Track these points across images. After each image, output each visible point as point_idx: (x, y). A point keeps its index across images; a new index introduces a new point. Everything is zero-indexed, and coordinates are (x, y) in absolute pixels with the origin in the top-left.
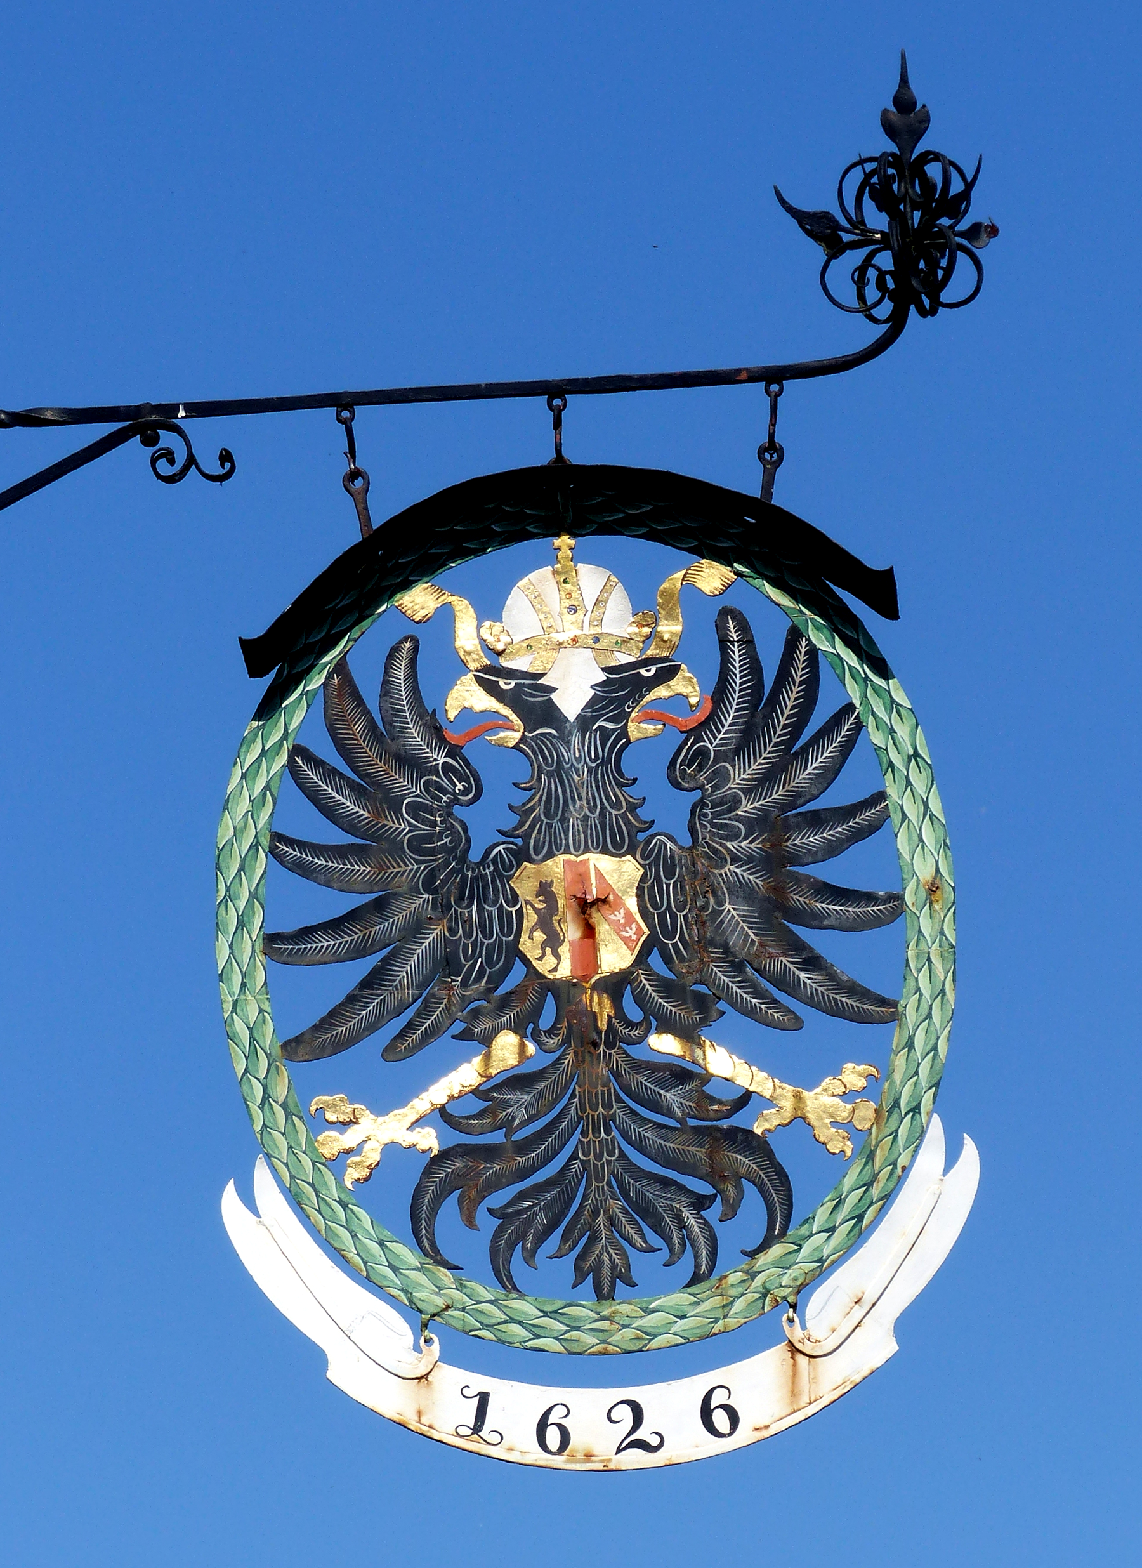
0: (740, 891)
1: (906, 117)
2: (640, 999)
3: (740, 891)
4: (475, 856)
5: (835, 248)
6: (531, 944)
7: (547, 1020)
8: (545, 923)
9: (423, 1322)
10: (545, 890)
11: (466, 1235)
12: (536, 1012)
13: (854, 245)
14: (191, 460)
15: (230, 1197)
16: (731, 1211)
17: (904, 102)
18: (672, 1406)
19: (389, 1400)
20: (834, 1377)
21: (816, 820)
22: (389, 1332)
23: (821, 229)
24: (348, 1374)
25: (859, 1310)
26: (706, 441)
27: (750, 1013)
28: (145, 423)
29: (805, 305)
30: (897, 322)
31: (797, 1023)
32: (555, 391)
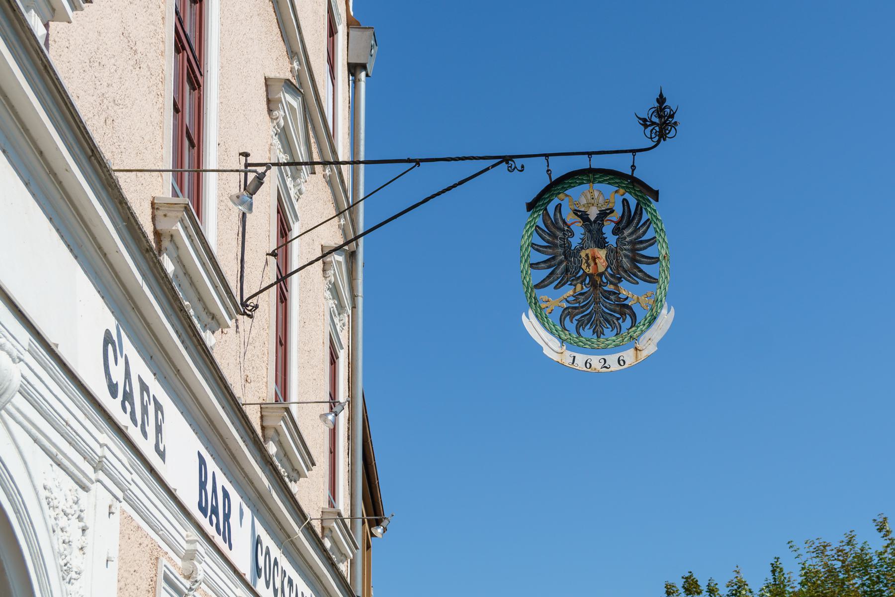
0: (626, 256)
1: (661, 100)
2: (606, 278)
3: (626, 256)
4: (573, 248)
5: (646, 126)
6: (584, 266)
7: (587, 281)
8: (587, 262)
9: (563, 341)
10: (587, 255)
11: (571, 325)
12: (585, 280)
13: (650, 125)
14: (515, 167)
15: (524, 316)
16: (624, 321)
17: (661, 95)
18: (612, 359)
19: (555, 357)
20: (643, 355)
21: (641, 242)
22: (555, 343)
23: (645, 123)
24: (547, 352)
25: (650, 342)
26: (622, 164)
27: (629, 281)
28: (506, 159)
29: (640, 138)
30: (659, 142)
31: (638, 283)
32: (589, 154)
